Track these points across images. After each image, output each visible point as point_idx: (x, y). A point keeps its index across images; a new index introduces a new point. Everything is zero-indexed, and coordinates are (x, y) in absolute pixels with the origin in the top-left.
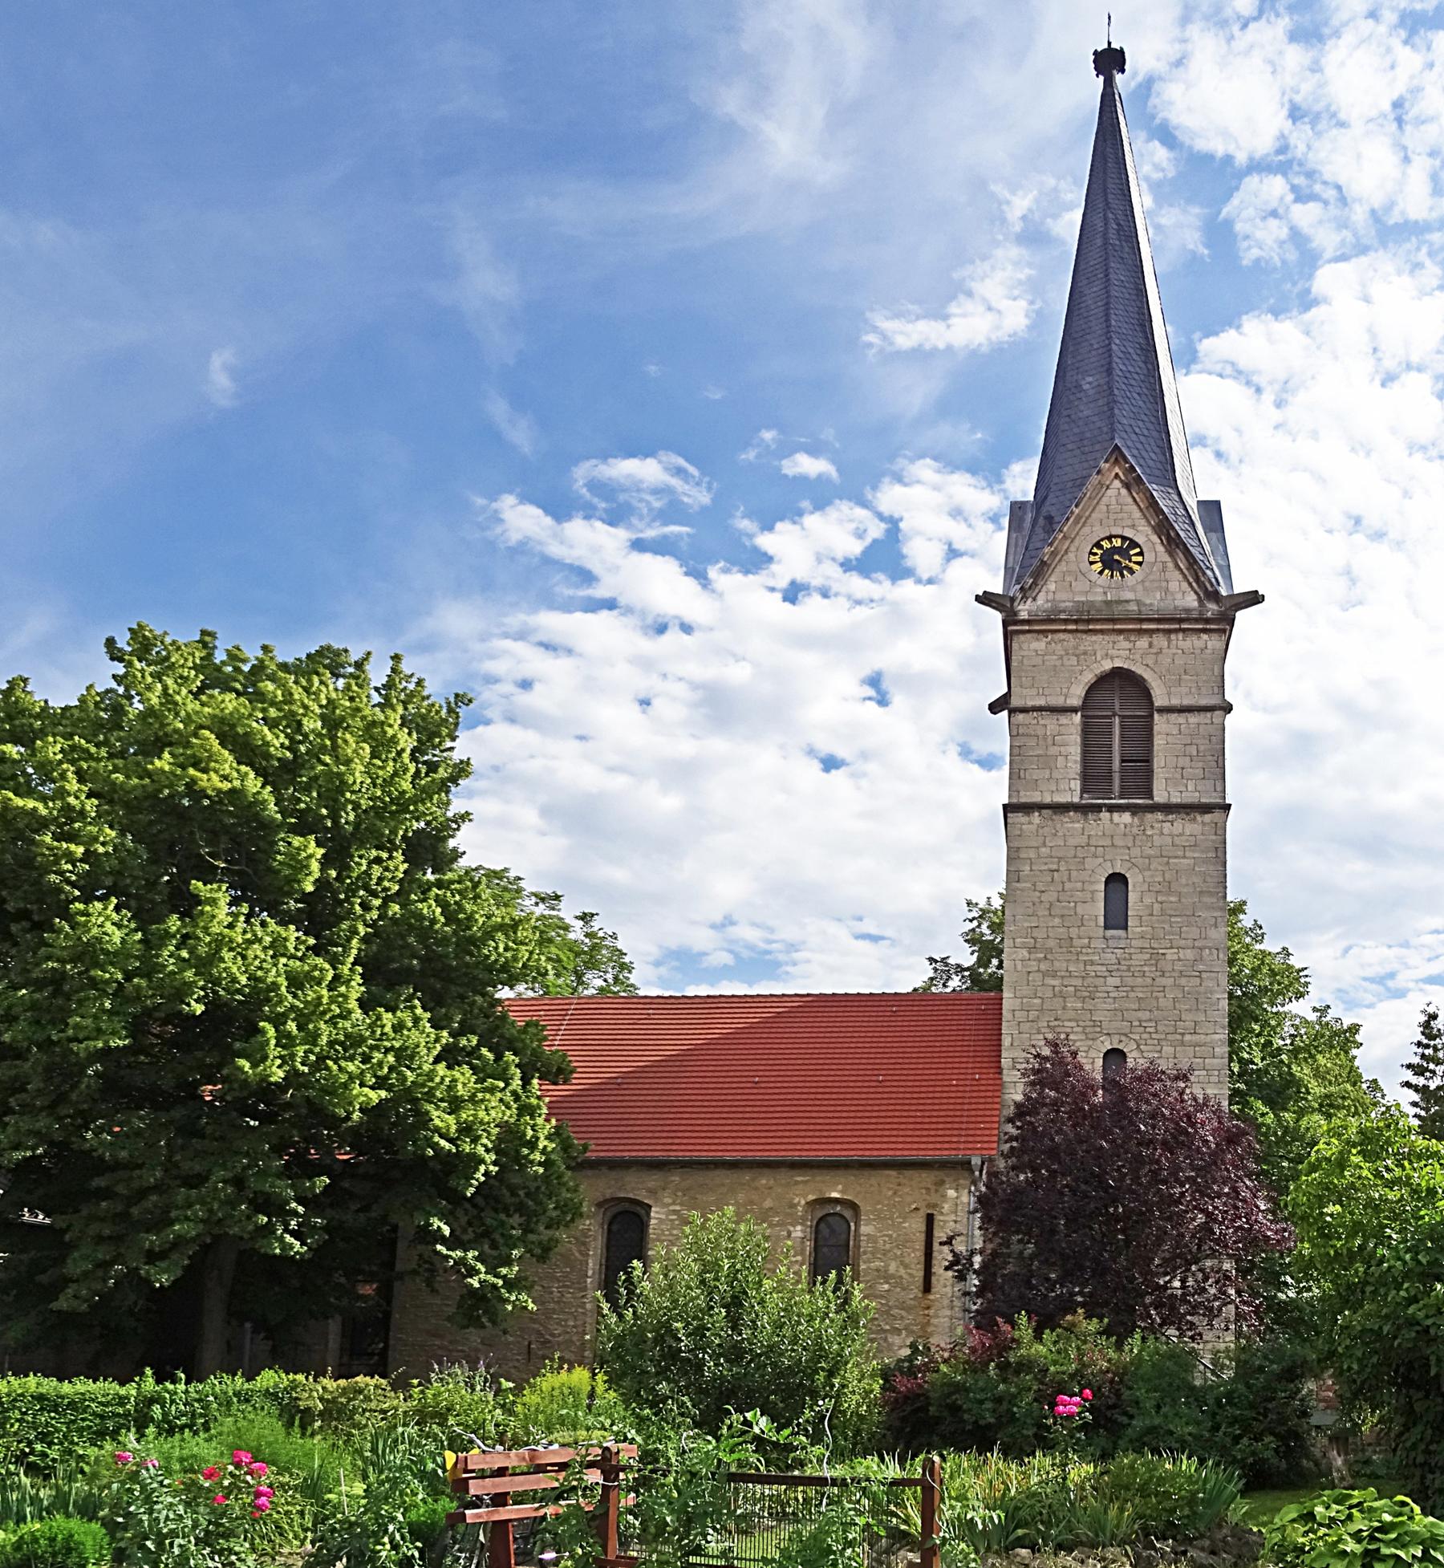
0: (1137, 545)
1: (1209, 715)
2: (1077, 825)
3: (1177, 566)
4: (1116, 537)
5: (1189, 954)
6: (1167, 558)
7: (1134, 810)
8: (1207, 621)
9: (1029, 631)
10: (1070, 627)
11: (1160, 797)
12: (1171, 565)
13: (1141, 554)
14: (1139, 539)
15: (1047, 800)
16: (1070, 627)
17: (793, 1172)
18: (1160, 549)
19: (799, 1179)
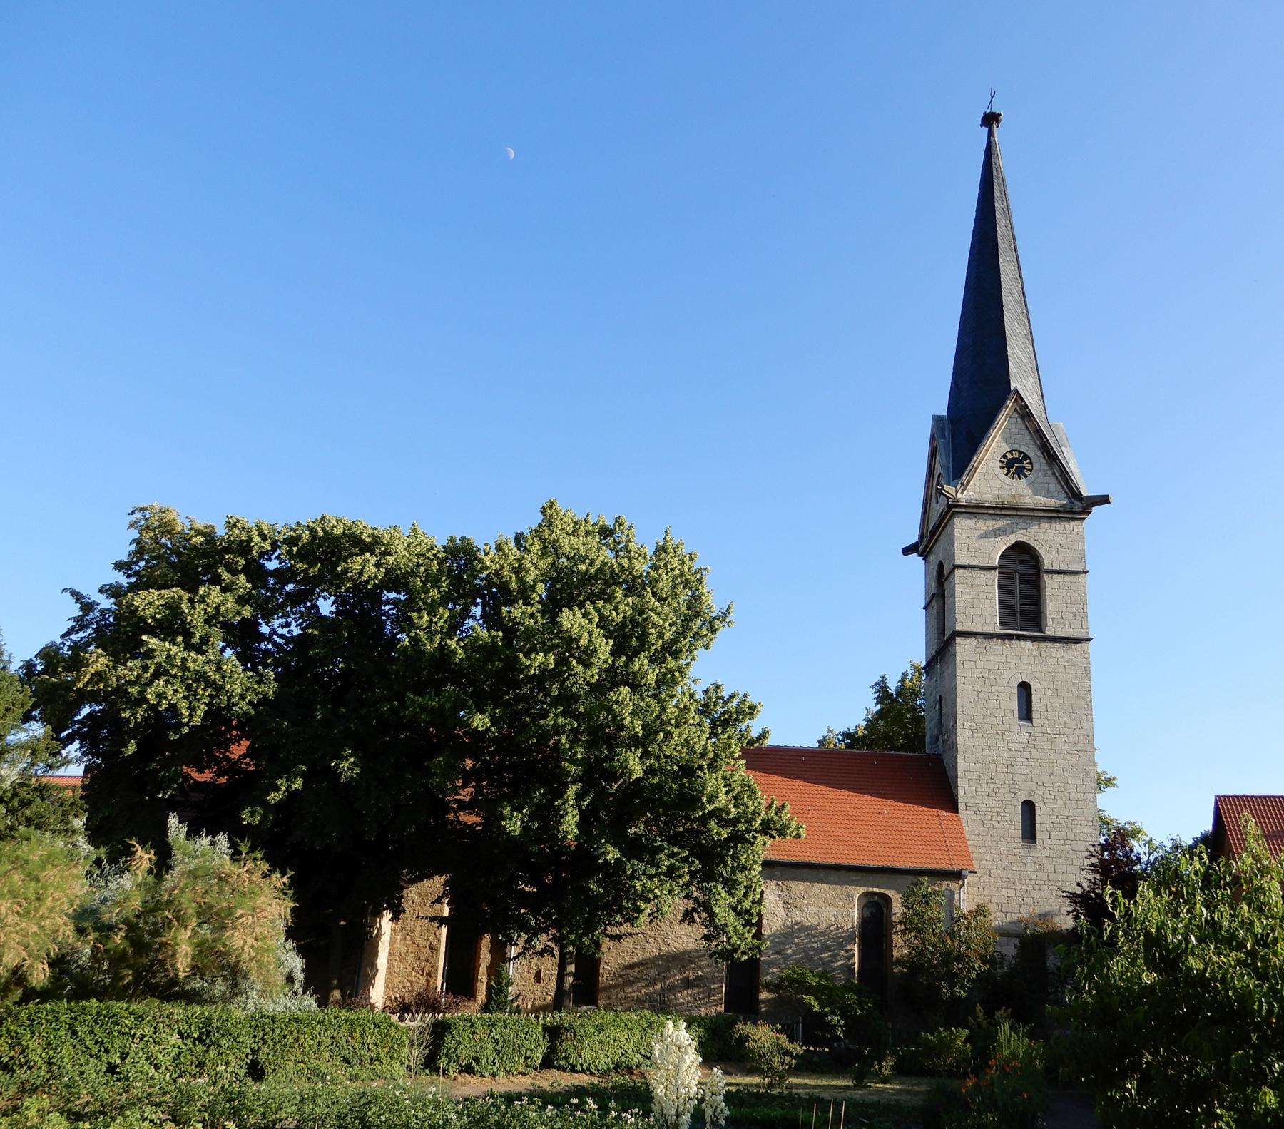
1: (1077, 576)
5: (1071, 739)
7: (1034, 639)
8: (1074, 513)
11: (1049, 632)
13: (1031, 463)
14: (1030, 454)
18: (1043, 461)
19: (854, 878)
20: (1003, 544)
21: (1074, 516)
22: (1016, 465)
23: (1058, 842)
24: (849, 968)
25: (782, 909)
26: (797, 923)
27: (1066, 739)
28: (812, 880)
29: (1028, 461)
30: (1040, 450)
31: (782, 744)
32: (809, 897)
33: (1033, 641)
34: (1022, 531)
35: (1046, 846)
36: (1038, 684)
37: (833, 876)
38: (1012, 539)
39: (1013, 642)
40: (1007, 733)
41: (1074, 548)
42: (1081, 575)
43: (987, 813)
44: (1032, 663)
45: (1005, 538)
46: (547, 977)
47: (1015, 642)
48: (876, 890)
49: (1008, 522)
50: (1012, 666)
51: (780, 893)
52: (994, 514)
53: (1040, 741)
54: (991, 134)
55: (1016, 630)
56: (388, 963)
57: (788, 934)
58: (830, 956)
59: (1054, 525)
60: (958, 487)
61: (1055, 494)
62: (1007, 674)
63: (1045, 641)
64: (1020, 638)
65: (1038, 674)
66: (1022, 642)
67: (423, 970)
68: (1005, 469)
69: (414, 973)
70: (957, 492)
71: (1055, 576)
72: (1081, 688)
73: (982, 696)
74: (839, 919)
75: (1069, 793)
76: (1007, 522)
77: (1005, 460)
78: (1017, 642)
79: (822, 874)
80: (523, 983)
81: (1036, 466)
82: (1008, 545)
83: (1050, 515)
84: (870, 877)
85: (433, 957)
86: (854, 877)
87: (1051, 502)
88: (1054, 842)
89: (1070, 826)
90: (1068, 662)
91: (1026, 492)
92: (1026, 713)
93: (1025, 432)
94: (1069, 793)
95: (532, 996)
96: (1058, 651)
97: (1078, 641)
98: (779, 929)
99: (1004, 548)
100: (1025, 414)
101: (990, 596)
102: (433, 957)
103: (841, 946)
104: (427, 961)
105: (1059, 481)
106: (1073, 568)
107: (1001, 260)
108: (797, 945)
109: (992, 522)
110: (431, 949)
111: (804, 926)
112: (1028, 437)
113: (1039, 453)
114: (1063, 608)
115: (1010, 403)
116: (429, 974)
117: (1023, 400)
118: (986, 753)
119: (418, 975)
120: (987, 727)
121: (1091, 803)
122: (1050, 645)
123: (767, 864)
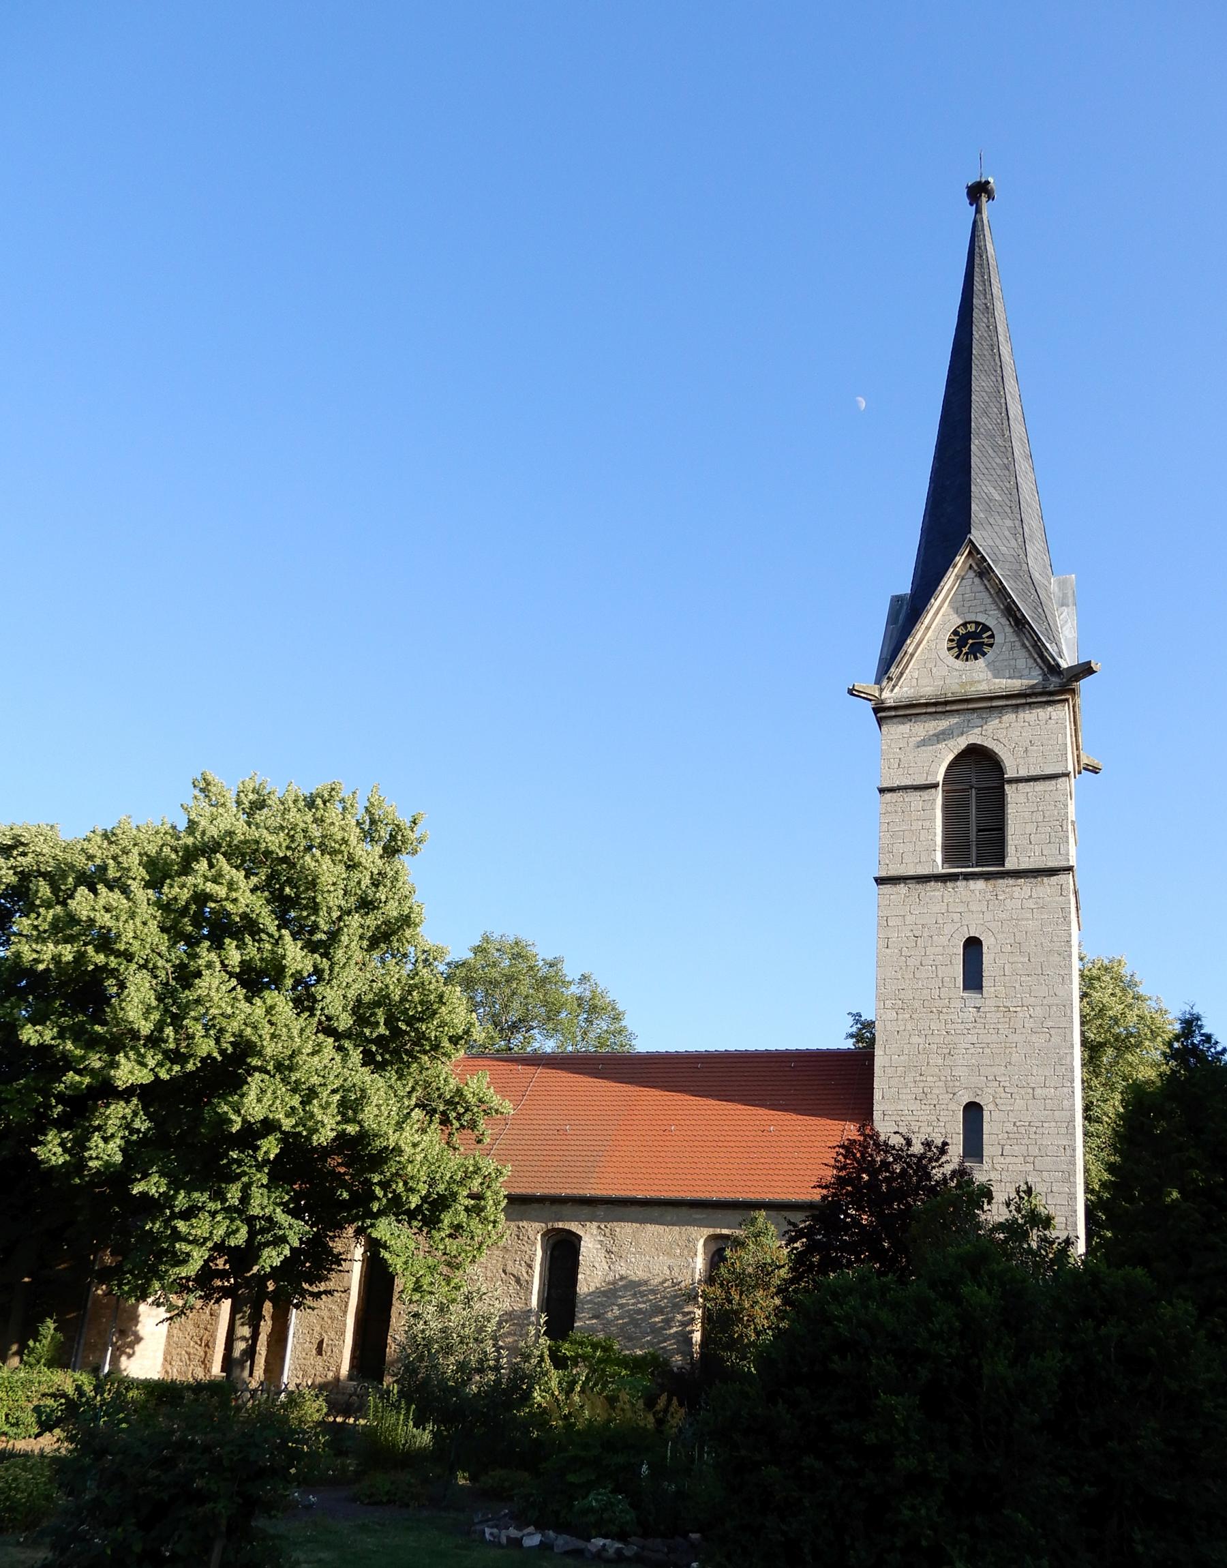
0: (988, 629)
1: (1053, 782)
2: (937, 893)
3: (1024, 645)
4: (969, 623)
5: (1038, 1012)
6: (1014, 638)
7: (987, 876)
8: (1051, 694)
9: (895, 716)
10: (930, 710)
11: (1011, 864)
12: (1018, 644)
13: (992, 636)
14: (991, 623)
15: (911, 873)
16: (930, 710)
17: (692, 1211)
18: (1009, 630)
19: (698, 1216)
20: (947, 754)
21: (1051, 698)
22: (970, 641)
23: (1014, 1160)
24: (686, 1339)
25: (603, 1259)
26: (622, 1278)
27: (1031, 1012)
28: (643, 1221)
29: (990, 633)
30: (1005, 616)
31: (682, 1049)
32: (638, 1243)
33: (987, 879)
34: (978, 730)
35: (997, 1166)
36: (993, 939)
37: (670, 1213)
38: (962, 743)
39: (959, 883)
40: (945, 1010)
41: (1051, 742)
42: (1060, 780)
43: (913, 1123)
44: (985, 909)
45: (951, 743)
46: (330, 1348)
47: (961, 884)
48: (725, 1231)
49: (956, 720)
50: (956, 917)
51: (602, 1238)
52: (936, 712)
53: (992, 1017)
54: (978, 211)
55: (969, 867)
56: (169, 1331)
57: (610, 1293)
58: (663, 1321)
59: (1021, 715)
60: (884, 683)
61: (1026, 672)
62: (948, 929)
63: (1003, 878)
64: (967, 877)
65: (992, 925)
66: (971, 882)
67: (201, 1340)
68: (956, 650)
69: (192, 1343)
70: (881, 690)
71: (1021, 785)
72: (1055, 939)
73: (911, 962)
74: (675, 1273)
75: (1033, 1089)
76: (954, 720)
77: (956, 638)
78: (964, 883)
79: (656, 1212)
80: (304, 1355)
81: (999, 639)
82: (956, 752)
83: (1014, 702)
84: (719, 1214)
85: (212, 1324)
86: (698, 1214)
87: (1016, 684)
88: (1008, 1160)
89: (1033, 1136)
90: (1037, 903)
91: (982, 676)
92: (973, 979)
93: (985, 595)
94: (1033, 1089)
95: (313, 1372)
96: (1022, 888)
97: (1052, 872)
98: (598, 1285)
99: (951, 757)
100: (983, 571)
101: (927, 824)
102: (212, 1324)
103: (677, 1307)
104: (206, 1329)
105: (1030, 654)
106: (1049, 771)
107: (974, 372)
108: (621, 1306)
109: (934, 723)
110: (211, 1315)
111: (631, 1281)
112: (990, 600)
113: (1004, 621)
114: (1030, 828)
115: (960, 560)
116: (207, 1345)
117: (979, 552)
118: (915, 1040)
119: (196, 1346)
120: (917, 1004)
121: (1065, 1102)
122: (1011, 881)
123: (513, 1199)
